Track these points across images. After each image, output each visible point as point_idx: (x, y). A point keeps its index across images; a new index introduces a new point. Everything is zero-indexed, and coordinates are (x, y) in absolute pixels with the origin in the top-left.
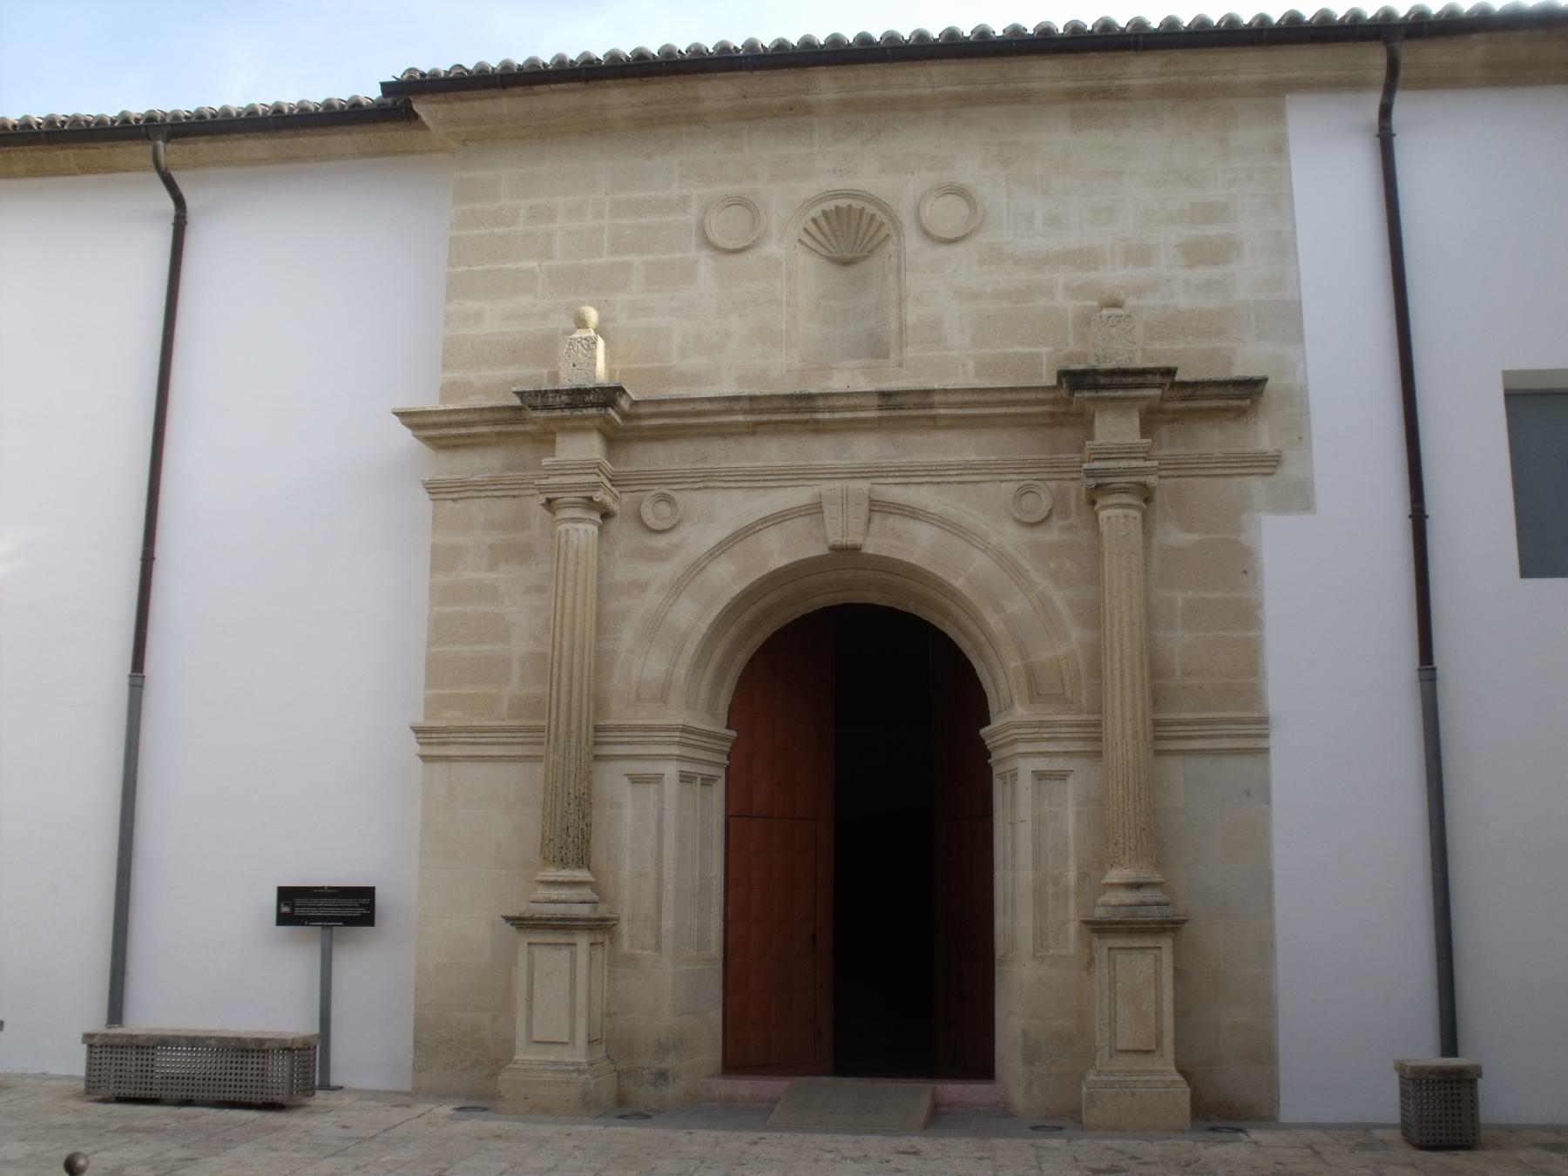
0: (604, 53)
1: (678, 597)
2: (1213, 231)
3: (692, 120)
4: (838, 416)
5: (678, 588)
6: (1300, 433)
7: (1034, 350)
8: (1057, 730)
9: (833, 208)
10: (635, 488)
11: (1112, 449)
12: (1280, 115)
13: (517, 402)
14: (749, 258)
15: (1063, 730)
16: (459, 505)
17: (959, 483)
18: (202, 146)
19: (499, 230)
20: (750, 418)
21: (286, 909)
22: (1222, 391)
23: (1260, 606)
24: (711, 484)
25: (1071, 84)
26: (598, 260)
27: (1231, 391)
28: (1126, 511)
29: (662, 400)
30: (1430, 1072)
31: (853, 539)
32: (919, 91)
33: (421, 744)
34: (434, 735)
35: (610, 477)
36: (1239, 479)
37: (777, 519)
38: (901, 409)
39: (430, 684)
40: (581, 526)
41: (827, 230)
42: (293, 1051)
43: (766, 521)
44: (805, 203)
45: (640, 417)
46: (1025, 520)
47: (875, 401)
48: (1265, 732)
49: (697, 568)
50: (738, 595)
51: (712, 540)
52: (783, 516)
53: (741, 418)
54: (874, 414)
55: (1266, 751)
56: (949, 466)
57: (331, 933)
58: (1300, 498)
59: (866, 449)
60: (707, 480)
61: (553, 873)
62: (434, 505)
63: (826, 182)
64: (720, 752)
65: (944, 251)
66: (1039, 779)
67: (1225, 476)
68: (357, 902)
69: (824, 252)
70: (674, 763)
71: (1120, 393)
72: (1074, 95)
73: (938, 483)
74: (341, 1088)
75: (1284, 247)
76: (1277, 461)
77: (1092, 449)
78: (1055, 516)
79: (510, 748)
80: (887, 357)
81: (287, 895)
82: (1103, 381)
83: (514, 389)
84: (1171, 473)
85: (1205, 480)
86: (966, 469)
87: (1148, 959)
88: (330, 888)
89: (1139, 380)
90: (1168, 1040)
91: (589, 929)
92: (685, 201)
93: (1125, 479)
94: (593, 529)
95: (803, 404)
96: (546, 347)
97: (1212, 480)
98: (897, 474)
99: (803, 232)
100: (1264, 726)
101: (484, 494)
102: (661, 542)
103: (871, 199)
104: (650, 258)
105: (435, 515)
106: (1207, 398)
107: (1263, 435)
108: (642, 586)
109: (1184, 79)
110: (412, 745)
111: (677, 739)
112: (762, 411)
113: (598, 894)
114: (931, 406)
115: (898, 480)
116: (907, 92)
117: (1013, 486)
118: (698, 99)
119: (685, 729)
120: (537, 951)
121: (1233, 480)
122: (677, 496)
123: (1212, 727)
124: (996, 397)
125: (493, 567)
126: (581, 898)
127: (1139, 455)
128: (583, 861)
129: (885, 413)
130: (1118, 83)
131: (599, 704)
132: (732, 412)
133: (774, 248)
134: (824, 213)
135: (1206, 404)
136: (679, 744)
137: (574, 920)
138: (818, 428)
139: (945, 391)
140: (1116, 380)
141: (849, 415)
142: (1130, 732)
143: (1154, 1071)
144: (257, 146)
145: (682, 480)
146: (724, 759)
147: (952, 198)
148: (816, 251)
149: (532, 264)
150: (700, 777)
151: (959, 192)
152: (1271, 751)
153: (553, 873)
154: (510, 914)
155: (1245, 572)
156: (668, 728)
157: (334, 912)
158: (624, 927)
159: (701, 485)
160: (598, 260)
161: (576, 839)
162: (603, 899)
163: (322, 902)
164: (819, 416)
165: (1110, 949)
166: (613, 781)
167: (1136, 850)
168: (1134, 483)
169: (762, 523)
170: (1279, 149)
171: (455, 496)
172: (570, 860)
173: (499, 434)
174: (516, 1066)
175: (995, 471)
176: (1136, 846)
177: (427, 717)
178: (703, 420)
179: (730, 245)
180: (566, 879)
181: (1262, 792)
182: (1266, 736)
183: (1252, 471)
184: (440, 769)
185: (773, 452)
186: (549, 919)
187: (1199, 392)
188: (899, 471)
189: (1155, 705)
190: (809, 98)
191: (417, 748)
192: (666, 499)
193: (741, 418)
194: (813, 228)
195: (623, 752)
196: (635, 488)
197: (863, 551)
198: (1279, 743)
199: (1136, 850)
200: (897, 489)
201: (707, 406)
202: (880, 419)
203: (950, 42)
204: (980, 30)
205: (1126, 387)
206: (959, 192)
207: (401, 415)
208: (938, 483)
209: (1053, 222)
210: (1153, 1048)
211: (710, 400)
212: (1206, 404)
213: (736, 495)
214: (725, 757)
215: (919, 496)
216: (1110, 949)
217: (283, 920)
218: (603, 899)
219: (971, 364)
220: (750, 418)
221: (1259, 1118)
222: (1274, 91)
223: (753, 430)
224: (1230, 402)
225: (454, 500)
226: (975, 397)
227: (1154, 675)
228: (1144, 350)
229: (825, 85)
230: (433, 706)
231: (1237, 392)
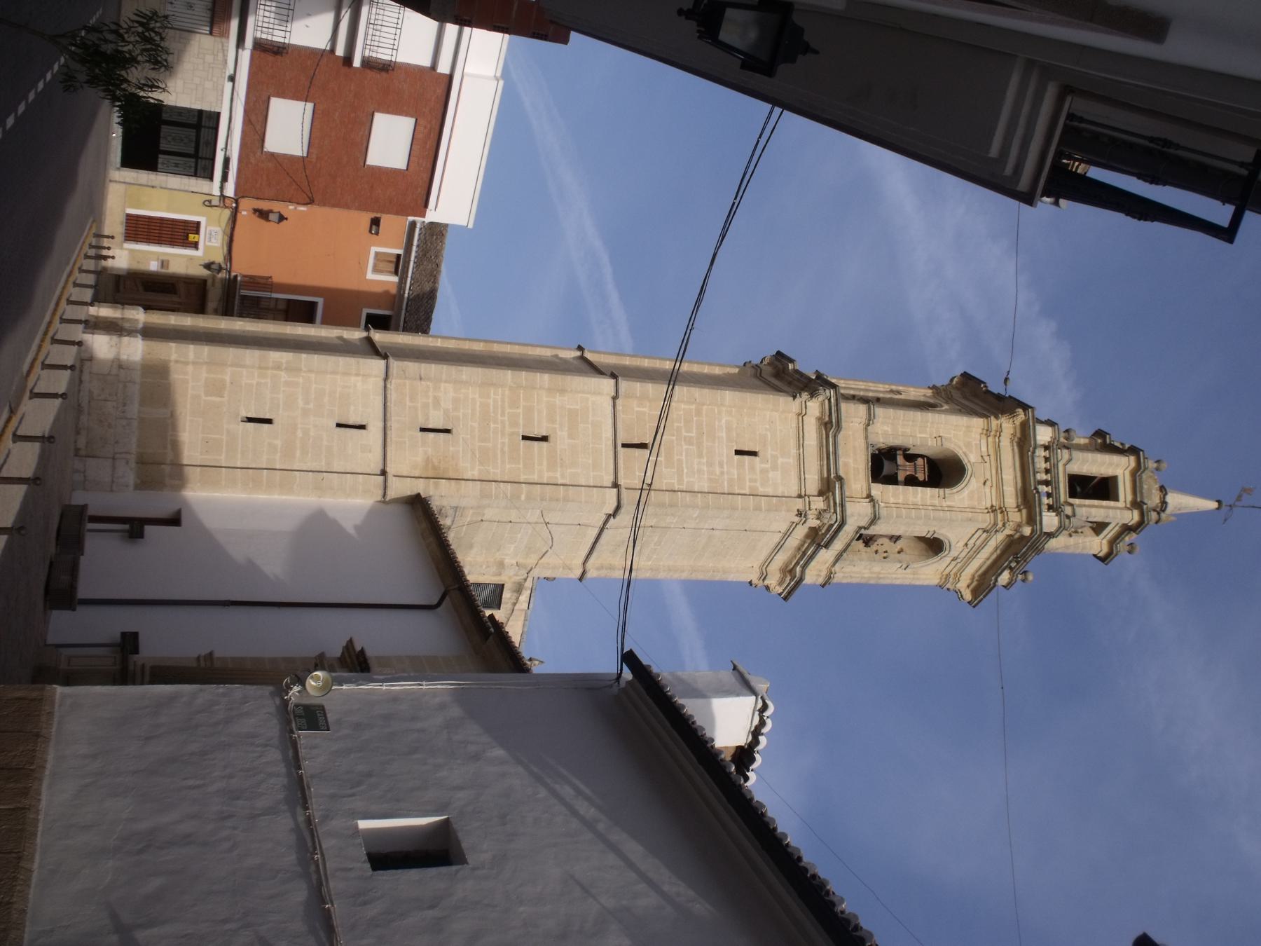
110: (204, 652)
177: (217, 658)
191: (203, 654)
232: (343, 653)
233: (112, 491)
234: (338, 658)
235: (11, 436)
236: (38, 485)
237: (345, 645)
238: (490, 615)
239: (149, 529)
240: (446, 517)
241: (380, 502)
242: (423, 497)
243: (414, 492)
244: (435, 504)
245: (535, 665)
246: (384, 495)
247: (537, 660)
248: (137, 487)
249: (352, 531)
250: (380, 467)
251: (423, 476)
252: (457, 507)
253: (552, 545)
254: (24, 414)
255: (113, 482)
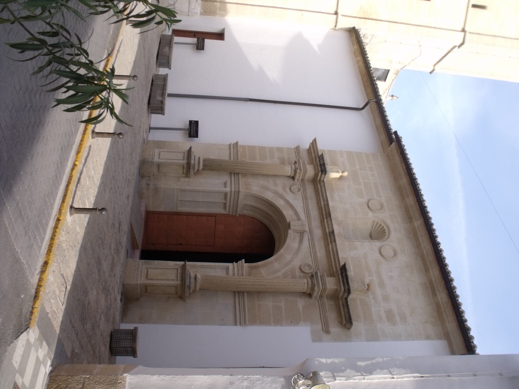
0: (442, 248)
1: (273, 193)
2: (398, 318)
3: (402, 197)
4: (326, 224)
5: (276, 193)
6: (338, 339)
7: (352, 271)
8: (241, 271)
9: (385, 228)
10: (301, 185)
11: (324, 279)
12: (439, 338)
13: (320, 154)
14: (367, 209)
15: (241, 272)
16: (294, 153)
17: (311, 252)
18: (377, 112)
19: (365, 161)
20: (323, 206)
21: (193, 122)
22: (347, 314)
23: (281, 326)
24: (304, 199)
25: (433, 280)
26: (361, 180)
27: (347, 316)
28: (306, 283)
29: (325, 187)
30: (135, 333)
31: (292, 227)
32: (422, 244)
33: (234, 144)
34: (236, 146)
35: (322, 296)
36: (320, 322)
37: (296, 213)
38: (330, 237)
39: (249, 147)
40: (290, 169)
41: (379, 229)
42: (164, 82)
43: (295, 211)
44: (385, 221)
45: (320, 184)
46: (301, 267)
47: (331, 230)
48: (242, 324)
49: (281, 197)
50: (275, 205)
51: (289, 199)
52: (297, 215)
53: (322, 204)
54: (327, 231)
55: (236, 325)
56: (315, 249)
57: (187, 130)
58: (316, 338)
59: (318, 232)
60: (305, 198)
61: (201, 161)
62: (293, 148)
63: (392, 226)
64: (233, 212)
65: (377, 252)
66: (226, 269)
67: (321, 318)
68: (195, 134)
69: (373, 230)
70: (230, 190)
71: (341, 280)
72: (431, 283)
73: (310, 247)
74: (149, 132)
75: (397, 337)
76: (327, 332)
77: (324, 274)
78: (303, 274)
79: (233, 156)
80: (344, 239)
81: (197, 123)
82: (344, 274)
83: (323, 153)
84: (320, 303)
85: (319, 312)
86: (315, 253)
87: (174, 278)
88: (198, 130)
89: (346, 283)
90: (150, 282)
91: (188, 163)
92: (380, 197)
93: (315, 281)
94: (289, 175)
95: (328, 215)
96: (334, 164)
97: (319, 314)
98: (311, 238)
99: (377, 222)
100: (243, 324)
101: (297, 156)
102: (288, 189)
103: (389, 236)
104: (363, 189)
105: (291, 148)
106: (344, 310)
107: (335, 329)
108: (276, 185)
109: (443, 309)
110: (233, 141)
111: (236, 190)
112: (325, 208)
113: (196, 172)
114: (331, 243)
115: (310, 238)
116: (421, 241)
117: (311, 263)
118: (408, 197)
119: (239, 192)
120: (175, 271)
121: (320, 320)
122: (300, 192)
123: (243, 310)
124: (336, 257)
125: (278, 158)
126: (195, 164)
127: (323, 286)
128: (204, 169)
129: (328, 234)
130: (437, 292)
131: (245, 175)
132: (324, 201)
133: (370, 214)
134: (383, 227)
135: (342, 310)
136: (235, 191)
137: (190, 159)
138: (322, 222)
139: (336, 245)
140: (345, 278)
141: (326, 226)
142: (241, 280)
143: (141, 277)
144: (379, 121)
145: (305, 193)
146: (231, 213)
147: (393, 253)
148: (372, 228)
149: (358, 167)
150: (226, 202)
151: (395, 254)
152: (236, 326)
153: (201, 161)
154: (192, 150)
155: (291, 322)
156: (239, 188)
157: (192, 130)
158: (187, 179)
159: (304, 197)
160: (361, 180)
161: (210, 164)
162: (195, 174)
163: (195, 128)
164: (325, 220)
165: (178, 269)
166: (225, 178)
167: (206, 279)
168: (315, 284)
169: (295, 210)
170: (428, 338)
171: (296, 151)
172: (205, 162)
173: (312, 159)
174: (154, 149)
175: (315, 260)
176: (207, 279)
177: (240, 145)
178: (321, 196)
179: (370, 206)
180: (200, 160)
181: (223, 323)
182: (240, 325)
183: (323, 326)
184: (228, 147)
185: (314, 213)
186: (190, 154)
187: (345, 307)
188: (312, 238)
189: (248, 292)
190: (414, 220)
191: (232, 143)
192: (299, 190)
193: (322, 204)
194: (378, 225)
195: (232, 179)
196: (301, 185)
197: (289, 230)
198: (238, 329)
199: (206, 279)
200: (307, 238)
201: (324, 196)
202: (326, 234)
203: (439, 251)
204: (442, 250)
205: (343, 281)
206: (395, 254)
207: (315, 140)
208: (310, 247)
209: (391, 278)
210: (148, 278)
211: (326, 196)
212: (342, 310)
213: (302, 205)
214: (231, 214)
215: (306, 243)
216: (178, 269)
217: (191, 122)
218: (195, 174)
219: (346, 256)
220: (323, 206)
221: (122, 319)
222: (446, 336)
223: (320, 208)
224: (344, 317)
225: (295, 152)
226: (325, 199)
227: (259, 292)
228: (357, 298)
229: (418, 223)
230: (243, 147)
231: (347, 318)
232: (310, 146)
233: (188, 15)
234: (308, 149)
235: (68, 210)
236: (135, 80)
237: (311, 142)
238: (395, 132)
239: (208, 42)
240: (367, 38)
241: (333, 29)
242: (356, 29)
243: (352, 26)
244: (362, 33)
245: (394, 99)
246: (336, 26)
247: (395, 96)
248: (202, 14)
249: (316, 48)
250: (335, 9)
251: (357, 16)
252: (373, 36)
253: (420, 56)
254: (90, 146)
255: (189, 11)
